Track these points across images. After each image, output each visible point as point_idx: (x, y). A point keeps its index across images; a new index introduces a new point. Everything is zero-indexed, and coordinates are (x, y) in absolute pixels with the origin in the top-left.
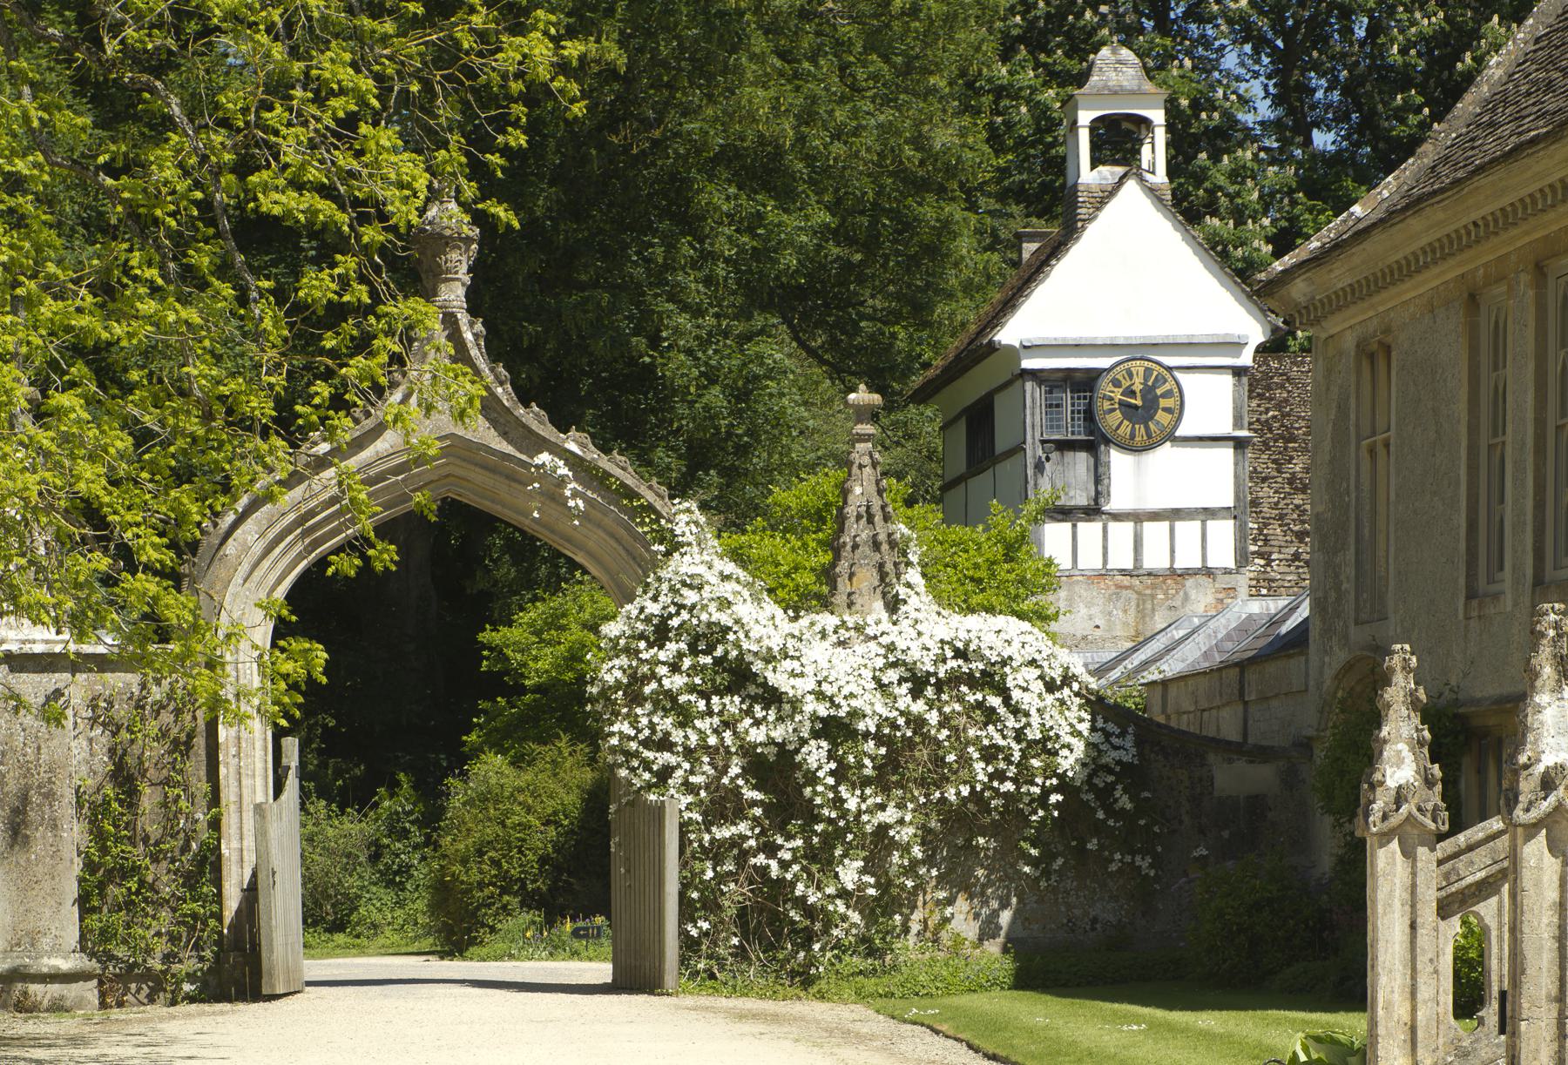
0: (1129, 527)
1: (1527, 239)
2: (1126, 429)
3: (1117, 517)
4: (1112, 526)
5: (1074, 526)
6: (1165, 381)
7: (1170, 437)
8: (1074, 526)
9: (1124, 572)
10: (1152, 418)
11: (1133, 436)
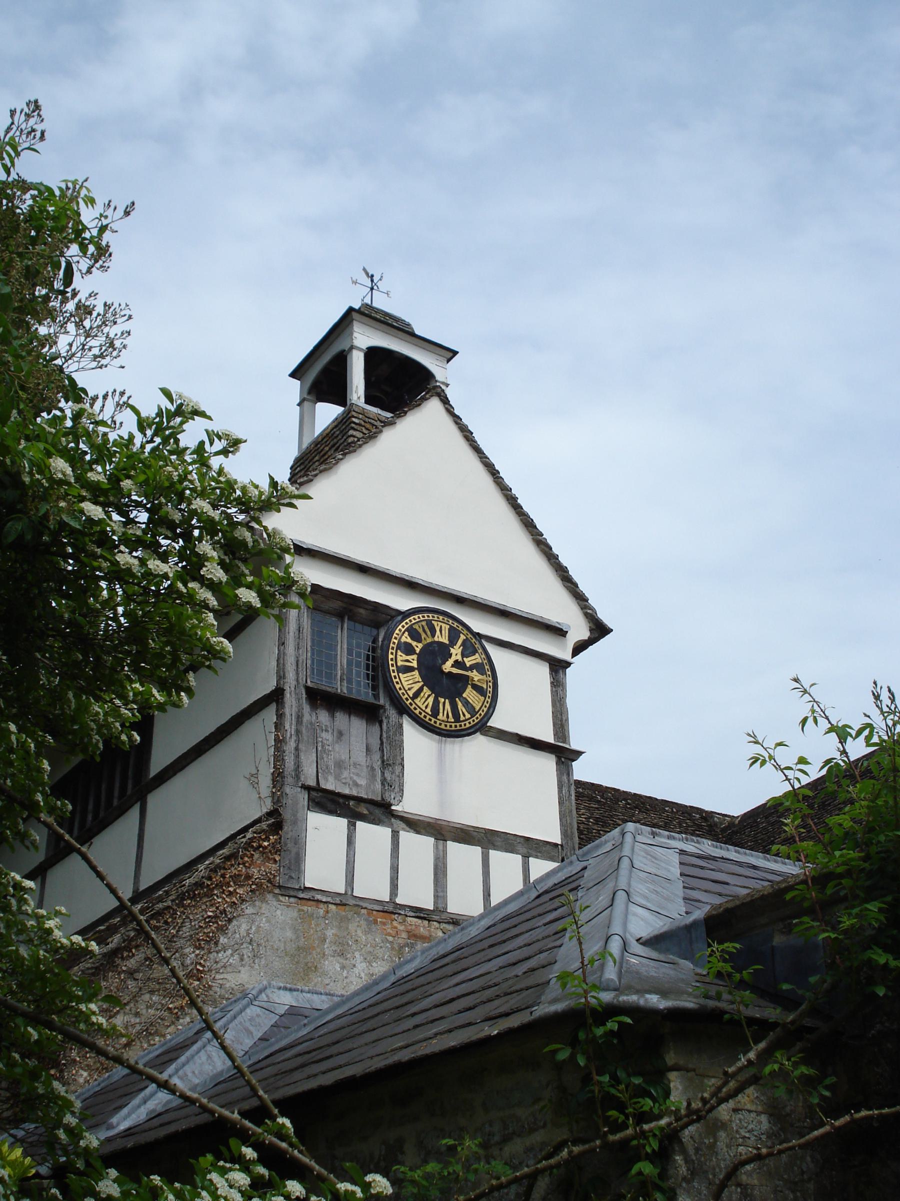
0: (476, 851)
1: (441, 711)
3: (416, 825)
4: (495, 855)
5: (352, 826)
6: (475, 652)
7: (482, 727)
8: (352, 826)
9: (419, 913)
10: (460, 695)
11: (435, 712)
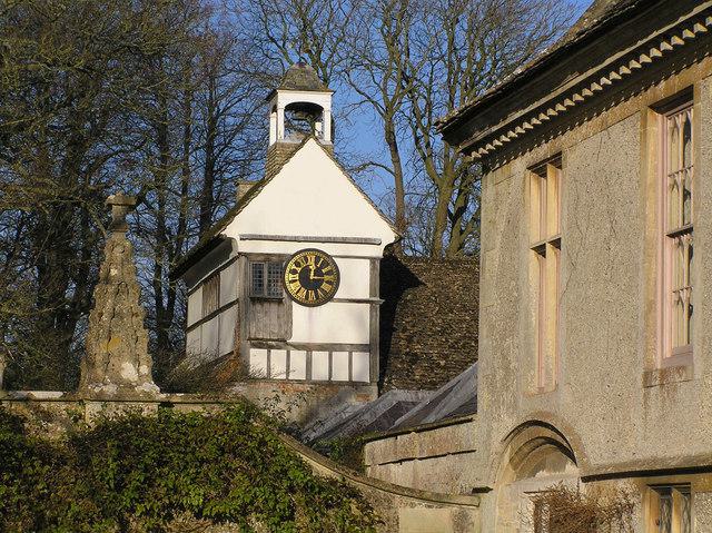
2: (303, 293)
4: (293, 353)
